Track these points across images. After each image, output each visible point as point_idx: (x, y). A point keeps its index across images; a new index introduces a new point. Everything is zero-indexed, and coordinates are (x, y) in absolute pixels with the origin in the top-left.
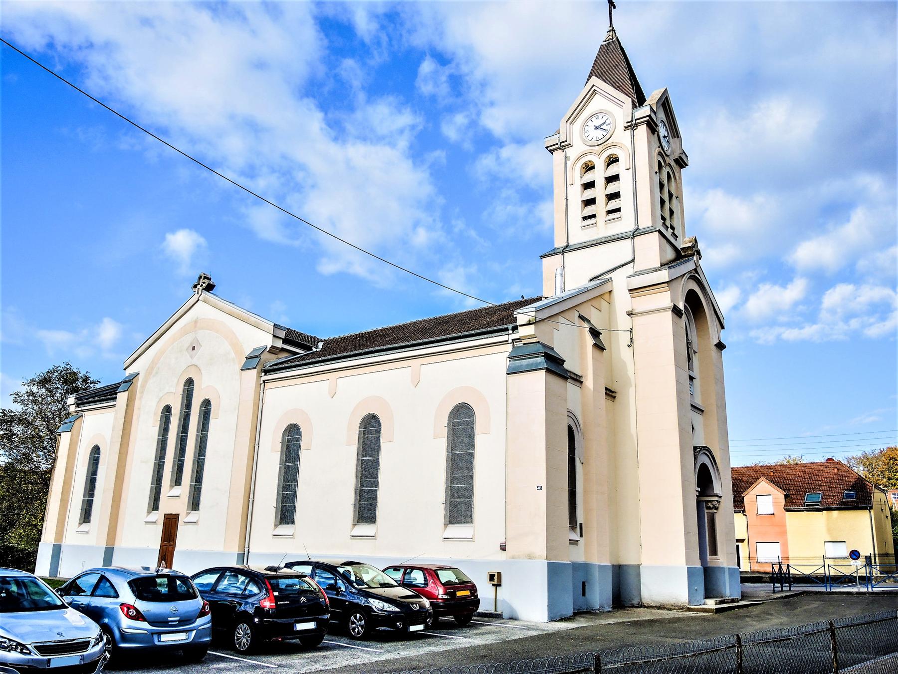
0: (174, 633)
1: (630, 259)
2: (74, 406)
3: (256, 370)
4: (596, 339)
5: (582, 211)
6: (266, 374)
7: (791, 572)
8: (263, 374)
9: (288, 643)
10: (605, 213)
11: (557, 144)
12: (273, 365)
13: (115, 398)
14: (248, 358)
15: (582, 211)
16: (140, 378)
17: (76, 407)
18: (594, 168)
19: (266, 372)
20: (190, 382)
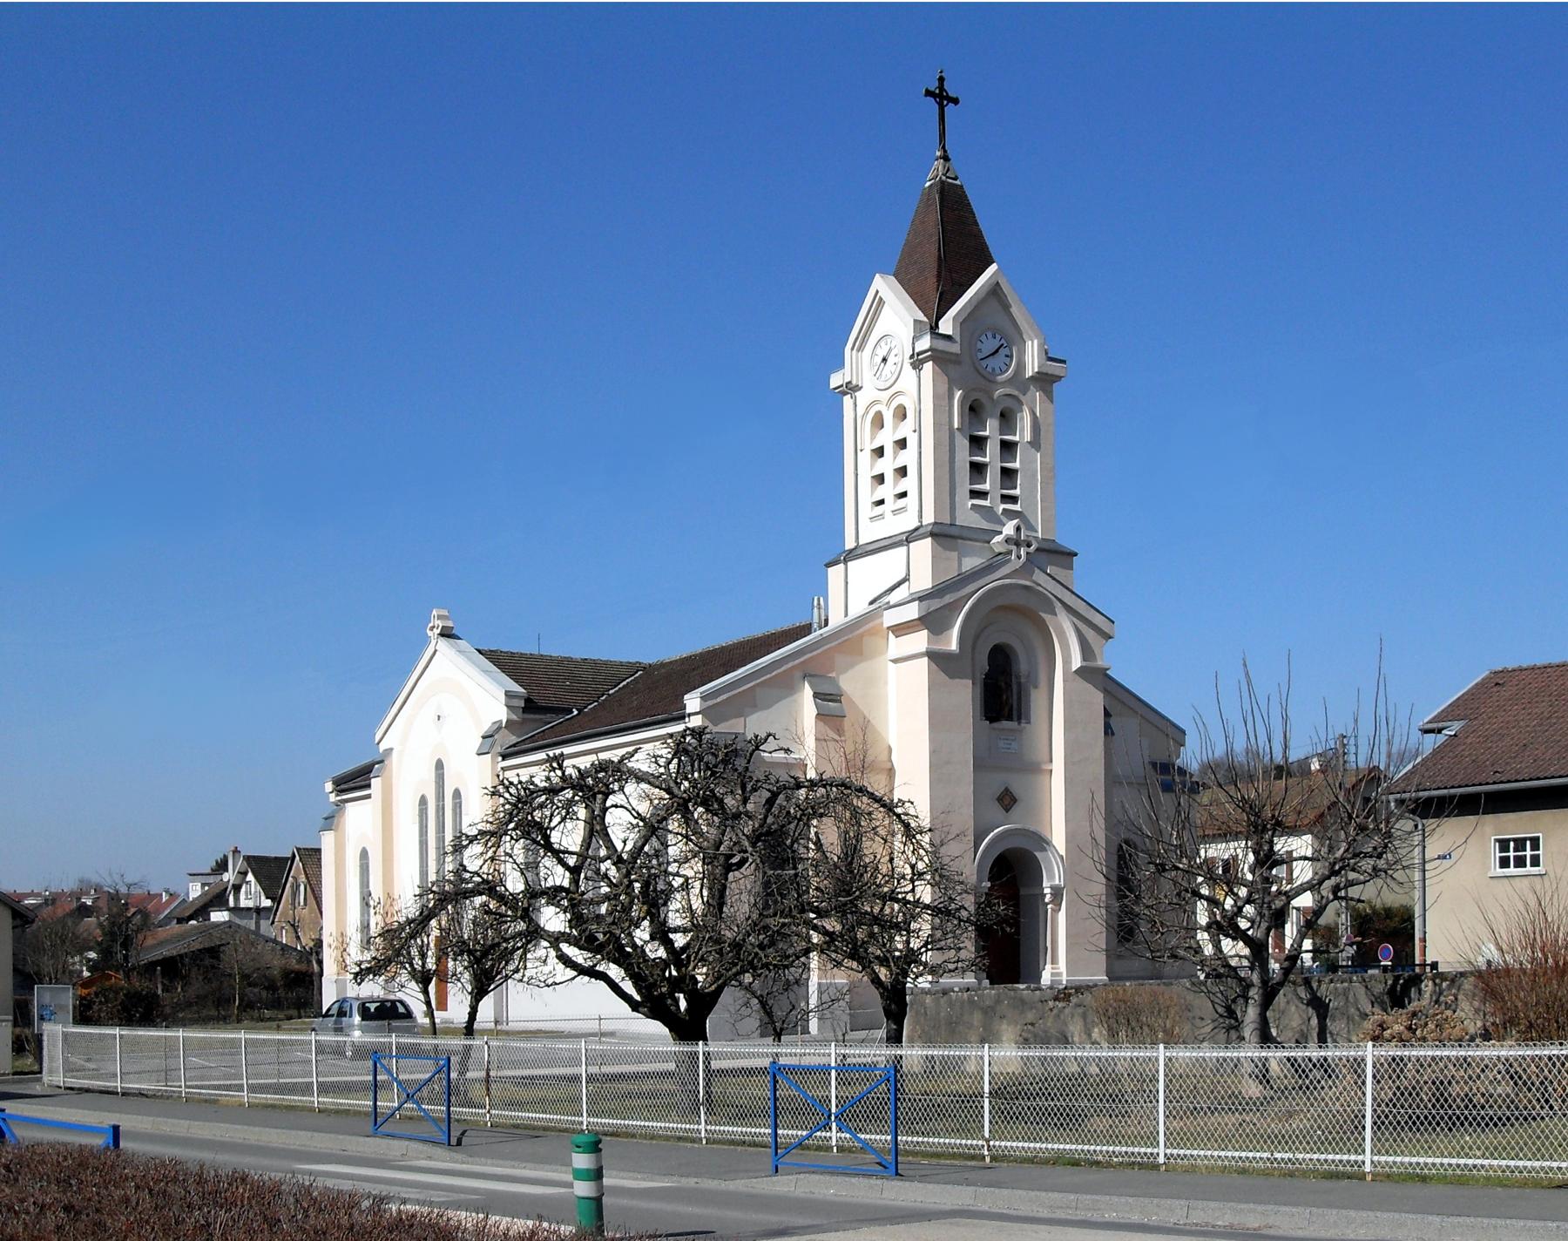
0: (1087, 619)
1: (903, 575)
2: (333, 794)
3: (489, 755)
4: (819, 722)
5: (872, 492)
6: (503, 760)
7: (1295, 863)
8: (500, 758)
9: (639, 991)
10: (893, 497)
11: (842, 386)
12: (514, 745)
13: (369, 786)
14: (484, 737)
15: (872, 492)
16: (394, 754)
17: (337, 795)
18: (119, 1126)
19: (505, 757)
20: (439, 765)
